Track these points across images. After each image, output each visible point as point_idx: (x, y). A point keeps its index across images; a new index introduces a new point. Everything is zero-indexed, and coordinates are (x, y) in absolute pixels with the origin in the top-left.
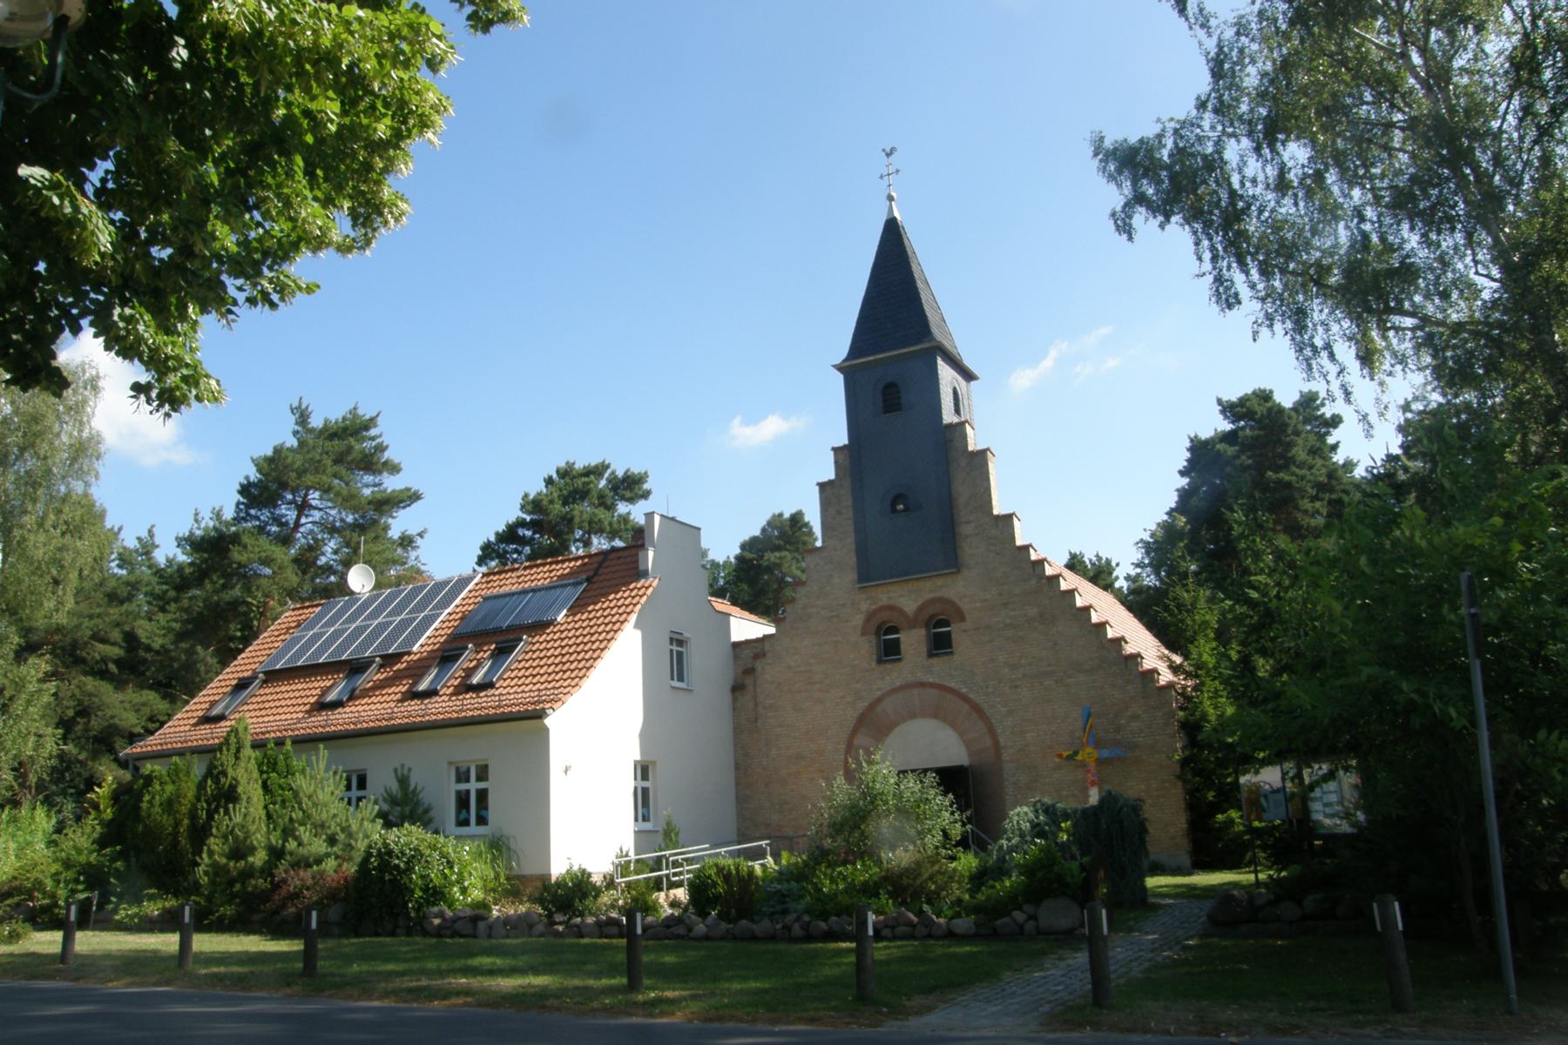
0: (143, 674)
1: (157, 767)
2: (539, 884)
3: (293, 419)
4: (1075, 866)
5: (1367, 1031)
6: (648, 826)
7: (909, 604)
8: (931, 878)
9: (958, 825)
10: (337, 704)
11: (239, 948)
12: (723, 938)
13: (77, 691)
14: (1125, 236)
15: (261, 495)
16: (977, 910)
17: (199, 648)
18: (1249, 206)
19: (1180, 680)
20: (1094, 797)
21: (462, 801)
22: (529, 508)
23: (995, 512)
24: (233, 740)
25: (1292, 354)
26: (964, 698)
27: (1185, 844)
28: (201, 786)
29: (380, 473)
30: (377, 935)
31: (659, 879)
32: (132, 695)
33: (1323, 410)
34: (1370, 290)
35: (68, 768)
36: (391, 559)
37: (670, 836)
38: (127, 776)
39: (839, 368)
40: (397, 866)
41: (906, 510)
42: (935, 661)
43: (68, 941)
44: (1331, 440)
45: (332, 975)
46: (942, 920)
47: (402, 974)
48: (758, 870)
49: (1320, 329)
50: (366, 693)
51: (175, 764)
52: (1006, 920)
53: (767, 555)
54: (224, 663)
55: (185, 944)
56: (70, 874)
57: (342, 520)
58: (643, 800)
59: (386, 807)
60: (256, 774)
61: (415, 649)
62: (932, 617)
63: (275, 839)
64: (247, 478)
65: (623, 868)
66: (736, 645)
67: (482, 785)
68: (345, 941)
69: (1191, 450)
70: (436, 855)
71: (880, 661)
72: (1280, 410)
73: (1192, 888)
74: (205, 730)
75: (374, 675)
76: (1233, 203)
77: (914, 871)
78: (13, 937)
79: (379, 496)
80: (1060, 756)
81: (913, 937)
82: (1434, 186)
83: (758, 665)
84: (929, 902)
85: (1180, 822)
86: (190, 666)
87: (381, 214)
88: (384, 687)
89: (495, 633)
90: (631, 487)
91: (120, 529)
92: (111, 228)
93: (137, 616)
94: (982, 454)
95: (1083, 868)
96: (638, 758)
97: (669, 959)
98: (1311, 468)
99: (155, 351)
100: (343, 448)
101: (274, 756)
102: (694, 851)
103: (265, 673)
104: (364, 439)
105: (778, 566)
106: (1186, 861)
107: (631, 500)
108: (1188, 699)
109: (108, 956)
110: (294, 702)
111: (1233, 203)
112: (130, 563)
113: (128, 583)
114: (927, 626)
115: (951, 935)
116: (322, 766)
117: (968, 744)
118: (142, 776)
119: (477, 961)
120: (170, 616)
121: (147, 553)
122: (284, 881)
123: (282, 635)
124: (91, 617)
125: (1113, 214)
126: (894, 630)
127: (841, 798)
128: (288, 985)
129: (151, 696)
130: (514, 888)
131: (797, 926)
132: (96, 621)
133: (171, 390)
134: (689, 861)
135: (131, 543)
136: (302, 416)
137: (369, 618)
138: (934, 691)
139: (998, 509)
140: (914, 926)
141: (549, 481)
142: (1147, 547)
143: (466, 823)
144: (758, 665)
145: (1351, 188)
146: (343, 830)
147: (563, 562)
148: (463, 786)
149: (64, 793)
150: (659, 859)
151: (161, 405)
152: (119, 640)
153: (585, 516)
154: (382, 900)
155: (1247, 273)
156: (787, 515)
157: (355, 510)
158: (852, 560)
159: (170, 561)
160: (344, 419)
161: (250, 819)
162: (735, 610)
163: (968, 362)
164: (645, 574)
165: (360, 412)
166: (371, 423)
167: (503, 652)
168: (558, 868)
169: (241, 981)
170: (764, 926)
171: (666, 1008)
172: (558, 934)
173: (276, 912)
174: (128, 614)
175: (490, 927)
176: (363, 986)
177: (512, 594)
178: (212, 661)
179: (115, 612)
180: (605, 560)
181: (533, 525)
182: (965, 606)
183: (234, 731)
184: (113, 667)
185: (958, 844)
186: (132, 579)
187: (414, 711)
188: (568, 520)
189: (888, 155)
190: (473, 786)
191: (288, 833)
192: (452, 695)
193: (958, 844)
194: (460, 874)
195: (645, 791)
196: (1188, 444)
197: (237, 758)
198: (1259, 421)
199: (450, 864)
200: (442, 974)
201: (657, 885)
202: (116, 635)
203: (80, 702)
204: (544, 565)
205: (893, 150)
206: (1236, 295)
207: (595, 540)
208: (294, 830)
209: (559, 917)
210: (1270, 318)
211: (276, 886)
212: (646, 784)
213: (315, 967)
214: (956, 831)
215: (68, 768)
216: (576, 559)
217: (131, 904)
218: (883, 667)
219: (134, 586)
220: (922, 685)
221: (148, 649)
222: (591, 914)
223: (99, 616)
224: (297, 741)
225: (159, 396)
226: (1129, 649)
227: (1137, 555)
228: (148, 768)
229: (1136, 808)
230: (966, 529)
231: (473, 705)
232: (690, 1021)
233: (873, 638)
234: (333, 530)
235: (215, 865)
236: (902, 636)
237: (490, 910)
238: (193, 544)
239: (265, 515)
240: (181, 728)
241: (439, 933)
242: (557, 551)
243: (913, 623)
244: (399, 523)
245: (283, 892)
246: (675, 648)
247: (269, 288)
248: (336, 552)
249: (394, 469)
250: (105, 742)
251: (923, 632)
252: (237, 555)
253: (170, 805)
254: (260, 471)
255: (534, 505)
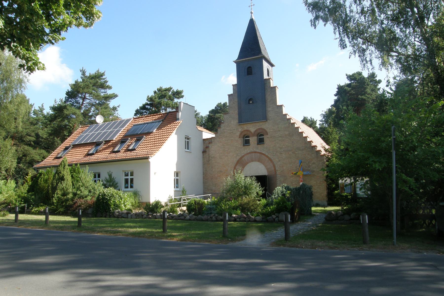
0: (41, 145)
1: (43, 171)
2: (145, 205)
3: (81, 73)
4: (290, 203)
5: (355, 249)
6: (178, 189)
7: (253, 130)
8: (252, 205)
9: (261, 191)
10: (92, 154)
11: (64, 220)
12: (194, 220)
13: (23, 150)
14: (313, 27)
15: (72, 94)
16: (263, 214)
17: (55, 138)
18: (350, 19)
19: (327, 153)
20: (301, 184)
21: (126, 181)
22: (149, 100)
23: (278, 104)
24: (63, 164)
25: (359, 63)
27: (326, 199)
28: (54, 176)
29: (106, 89)
30: (102, 217)
31: (180, 203)
32: (38, 151)
33: (376, 78)
34: (386, 44)
35: (21, 171)
36: (110, 114)
37: (184, 192)
38: (35, 172)
39: (235, 62)
40: (107, 199)
41: (253, 103)
42: (259, 146)
43: (16, 217)
44: (378, 87)
45: (86, 227)
46: (253, 217)
47: (107, 227)
48: (206, 202)
49: (369, 55)
50: (100, 151)
51: (48, 170)
52: (270, 217)
53: (217, 115)
54: (62, 142)
55: (47, 218)
56: (20, 199)
57: (95, 102)
58: (177, 182)
59: (105, 183)
60: (69, 173)
61: (114, 139)
62: (259, 133)
63: (75, 191)
64: (68, 90)
65: (171, 201)
66: (204, 140)
67: (132, 177)
68: (92, 219)
69: (338, 88)
70: (117, 196)
71: (244, 145)
72: (364, 78)
73: (325, 211)
74: (56, 161)
75: (102, 146)
76: (346, 18)
77: (248, 204)
78: (4, 215)
79: (106, 96)
80: (293, 173)
81: (245, 221)
82: (405, 14)
83: (210, 145)
84: (251, 212)
85: (325, 193)
86: (53, 143)
87: (93, 17)
88: (105, 150)
89: (137, 135)
90: (178, 94)
91: (34, 104)
92: (3, 21)
93: (39, 129)
94: (275, 88)
95: (292, 204)
97: (178, 225)
98: (371, 95)
99: (24, 55)
100: (95, 82)
101: (74, 169)
102: (190, 196)
103: (73, 145)
104: (101, 79)
105: (220, 118)
106: (326, 203)
107: (178, 98)
108: (329, 159)
109: (28, 221)
110: (81, 153)
111: (346, 18)
112: (37, 114)
113: (36, 120)
114: (257, 136)
115: (255, 221)
116: (87, 171)
117: (267, 169)
118: (39, 173)
119: (125, 224)
120: (48, 129)
121: (42, 111)
122: (76, 202)
123: (79, 134)
124: (26, 129)
125: (311, 21)
126: (248, 137)
127: (229, 183)
128: (73, 229)
129: (43, 151)
130: (140, 205)
131: (214, 217)
132: (28, 130)
133: (30, 67)
134: (188, 199)
135: (37, 108)
136: (83, 73)
137: (114, 128)
138: (259, 154)
139: (278, 104)
140: (245, 218)
141: (155, 92)
142: (324, 116)
143: (127, 187)
144: (210, 145)
145: (381, 14)
146: (93, 189)
147: (156, 115)
148: (127, 177)
149: (20, 177)
150: (181, 198)
151: (28, 71)
152: (34, 136)
153: (165, 103)
154: (102, 208)
155: (349, 39)
156: (222, 103)
157: (98, 99)
158: (237, 117)
159: (48, 113)
160: (95, 73)
161: (68, 185)
162: (205, 130)
163: (272, 61)
164: (178, 119)
165: (100, 71)
166: (102, 75)
167: (138, 140)
168: (152, 200)
169: (61, 228)
170: (205, 217)
171: (172, 238)
172: (150, 218)
173: (74, 211)
174: (36, 128)
175: (132, 216)
176: (93, 230)
177: (141, 124)
178: (59, 142)
179: (32, 128)
180: (167, 115)
181: (151, 105)
182: (268, 130)
183: (63, 161)
184: (32, 143)
185: (261, 196)
186: (37, 118)
187: (114, 156)
188: (160, 103)
190: (129, 177)
191: (78, 189)
192: (124, 152)
193: (261, 196)
194: (124, 201)
195: (177, 180)
196: (337, 87)
197: (64, 169)
198: (357, 81)
199: (121, 198)
200: (115, 227)
201: (180, 206)
202: (33, 134)
203: (24, 153)
204: (150, 116)
206: (346, 45)
207: (168, 109)
208: (79, 188)
209: (150, 213)
210: (355, 52)
211: (75, 203)
212: (177, 178)
213: (81, 225)
214: (261, 193)
215: (21, 171)
216: (161, 114)
217: (36, 207)
218: (244, 147)
219: (38, 120)
220: (255, 152)
221: (42, 138)
222: (159, 213)
223: (28, 129)
224: (81, 164)
225: (27, 68)
226: (313, 144)
227: (321, 118)
228: (40, 171)
229: (310, 188)
230: (269, 109)
231: (130, 155)
232: (178, 241)
233: (242, 139)
234: (92, 105)
235: (58, 197)
236: (250, 138)
237: (132, 211)
238: (53, 108)
239: (73, 100)
240: (50, 160)
241: (118, 217)
242: (156, 112)
243: (253, 135)
244: (112, 103)
245: (76, 205)
246: (187, 140)
247: (51, 39)
248: (94, 111)
249: (110, 88)
250: (31, 163)
251: (256, 137)
252: (65, 112)
253: (46, 181)
254: (71, 88)
255: (150, 99)
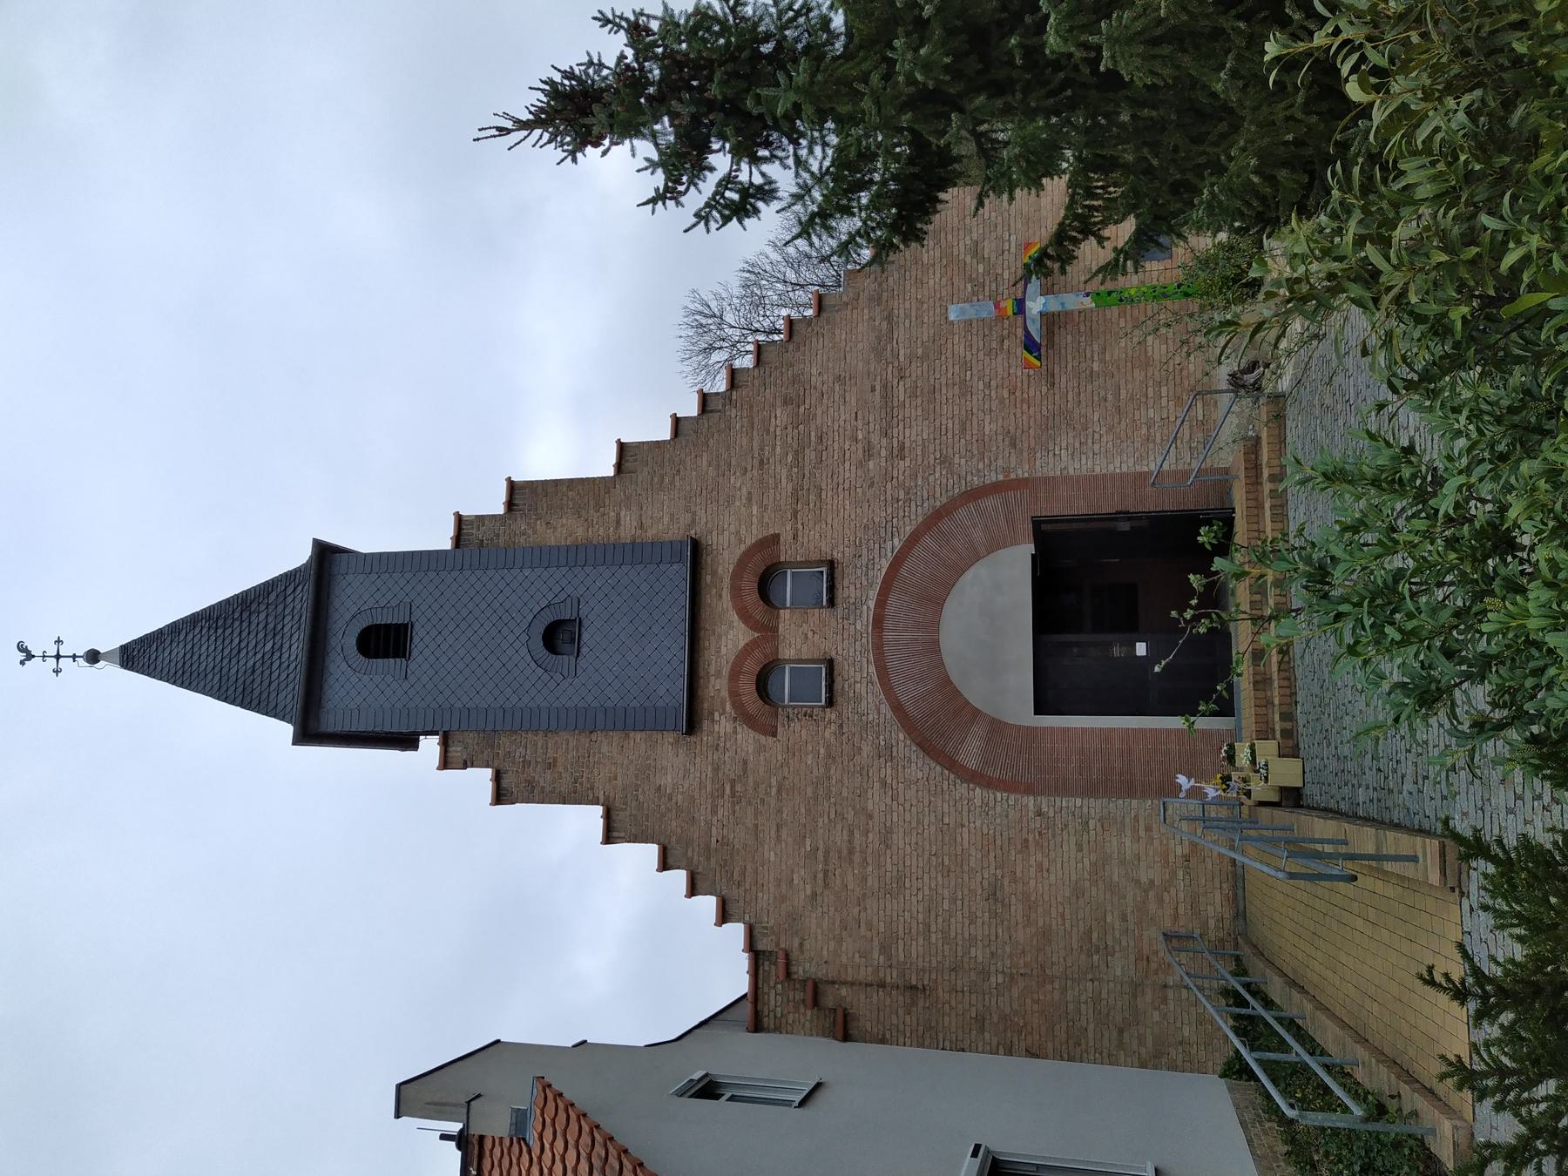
26: (913, 540)
96: (286, 730)
117: (994, 546)
138: (892, 600)
182: (753, 536)
189: (30, 656)
205: (22, 648)
220: (878, 622)
